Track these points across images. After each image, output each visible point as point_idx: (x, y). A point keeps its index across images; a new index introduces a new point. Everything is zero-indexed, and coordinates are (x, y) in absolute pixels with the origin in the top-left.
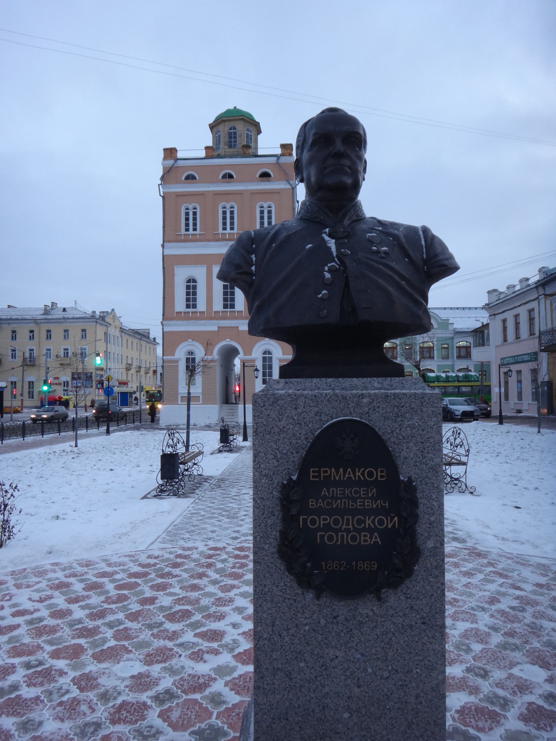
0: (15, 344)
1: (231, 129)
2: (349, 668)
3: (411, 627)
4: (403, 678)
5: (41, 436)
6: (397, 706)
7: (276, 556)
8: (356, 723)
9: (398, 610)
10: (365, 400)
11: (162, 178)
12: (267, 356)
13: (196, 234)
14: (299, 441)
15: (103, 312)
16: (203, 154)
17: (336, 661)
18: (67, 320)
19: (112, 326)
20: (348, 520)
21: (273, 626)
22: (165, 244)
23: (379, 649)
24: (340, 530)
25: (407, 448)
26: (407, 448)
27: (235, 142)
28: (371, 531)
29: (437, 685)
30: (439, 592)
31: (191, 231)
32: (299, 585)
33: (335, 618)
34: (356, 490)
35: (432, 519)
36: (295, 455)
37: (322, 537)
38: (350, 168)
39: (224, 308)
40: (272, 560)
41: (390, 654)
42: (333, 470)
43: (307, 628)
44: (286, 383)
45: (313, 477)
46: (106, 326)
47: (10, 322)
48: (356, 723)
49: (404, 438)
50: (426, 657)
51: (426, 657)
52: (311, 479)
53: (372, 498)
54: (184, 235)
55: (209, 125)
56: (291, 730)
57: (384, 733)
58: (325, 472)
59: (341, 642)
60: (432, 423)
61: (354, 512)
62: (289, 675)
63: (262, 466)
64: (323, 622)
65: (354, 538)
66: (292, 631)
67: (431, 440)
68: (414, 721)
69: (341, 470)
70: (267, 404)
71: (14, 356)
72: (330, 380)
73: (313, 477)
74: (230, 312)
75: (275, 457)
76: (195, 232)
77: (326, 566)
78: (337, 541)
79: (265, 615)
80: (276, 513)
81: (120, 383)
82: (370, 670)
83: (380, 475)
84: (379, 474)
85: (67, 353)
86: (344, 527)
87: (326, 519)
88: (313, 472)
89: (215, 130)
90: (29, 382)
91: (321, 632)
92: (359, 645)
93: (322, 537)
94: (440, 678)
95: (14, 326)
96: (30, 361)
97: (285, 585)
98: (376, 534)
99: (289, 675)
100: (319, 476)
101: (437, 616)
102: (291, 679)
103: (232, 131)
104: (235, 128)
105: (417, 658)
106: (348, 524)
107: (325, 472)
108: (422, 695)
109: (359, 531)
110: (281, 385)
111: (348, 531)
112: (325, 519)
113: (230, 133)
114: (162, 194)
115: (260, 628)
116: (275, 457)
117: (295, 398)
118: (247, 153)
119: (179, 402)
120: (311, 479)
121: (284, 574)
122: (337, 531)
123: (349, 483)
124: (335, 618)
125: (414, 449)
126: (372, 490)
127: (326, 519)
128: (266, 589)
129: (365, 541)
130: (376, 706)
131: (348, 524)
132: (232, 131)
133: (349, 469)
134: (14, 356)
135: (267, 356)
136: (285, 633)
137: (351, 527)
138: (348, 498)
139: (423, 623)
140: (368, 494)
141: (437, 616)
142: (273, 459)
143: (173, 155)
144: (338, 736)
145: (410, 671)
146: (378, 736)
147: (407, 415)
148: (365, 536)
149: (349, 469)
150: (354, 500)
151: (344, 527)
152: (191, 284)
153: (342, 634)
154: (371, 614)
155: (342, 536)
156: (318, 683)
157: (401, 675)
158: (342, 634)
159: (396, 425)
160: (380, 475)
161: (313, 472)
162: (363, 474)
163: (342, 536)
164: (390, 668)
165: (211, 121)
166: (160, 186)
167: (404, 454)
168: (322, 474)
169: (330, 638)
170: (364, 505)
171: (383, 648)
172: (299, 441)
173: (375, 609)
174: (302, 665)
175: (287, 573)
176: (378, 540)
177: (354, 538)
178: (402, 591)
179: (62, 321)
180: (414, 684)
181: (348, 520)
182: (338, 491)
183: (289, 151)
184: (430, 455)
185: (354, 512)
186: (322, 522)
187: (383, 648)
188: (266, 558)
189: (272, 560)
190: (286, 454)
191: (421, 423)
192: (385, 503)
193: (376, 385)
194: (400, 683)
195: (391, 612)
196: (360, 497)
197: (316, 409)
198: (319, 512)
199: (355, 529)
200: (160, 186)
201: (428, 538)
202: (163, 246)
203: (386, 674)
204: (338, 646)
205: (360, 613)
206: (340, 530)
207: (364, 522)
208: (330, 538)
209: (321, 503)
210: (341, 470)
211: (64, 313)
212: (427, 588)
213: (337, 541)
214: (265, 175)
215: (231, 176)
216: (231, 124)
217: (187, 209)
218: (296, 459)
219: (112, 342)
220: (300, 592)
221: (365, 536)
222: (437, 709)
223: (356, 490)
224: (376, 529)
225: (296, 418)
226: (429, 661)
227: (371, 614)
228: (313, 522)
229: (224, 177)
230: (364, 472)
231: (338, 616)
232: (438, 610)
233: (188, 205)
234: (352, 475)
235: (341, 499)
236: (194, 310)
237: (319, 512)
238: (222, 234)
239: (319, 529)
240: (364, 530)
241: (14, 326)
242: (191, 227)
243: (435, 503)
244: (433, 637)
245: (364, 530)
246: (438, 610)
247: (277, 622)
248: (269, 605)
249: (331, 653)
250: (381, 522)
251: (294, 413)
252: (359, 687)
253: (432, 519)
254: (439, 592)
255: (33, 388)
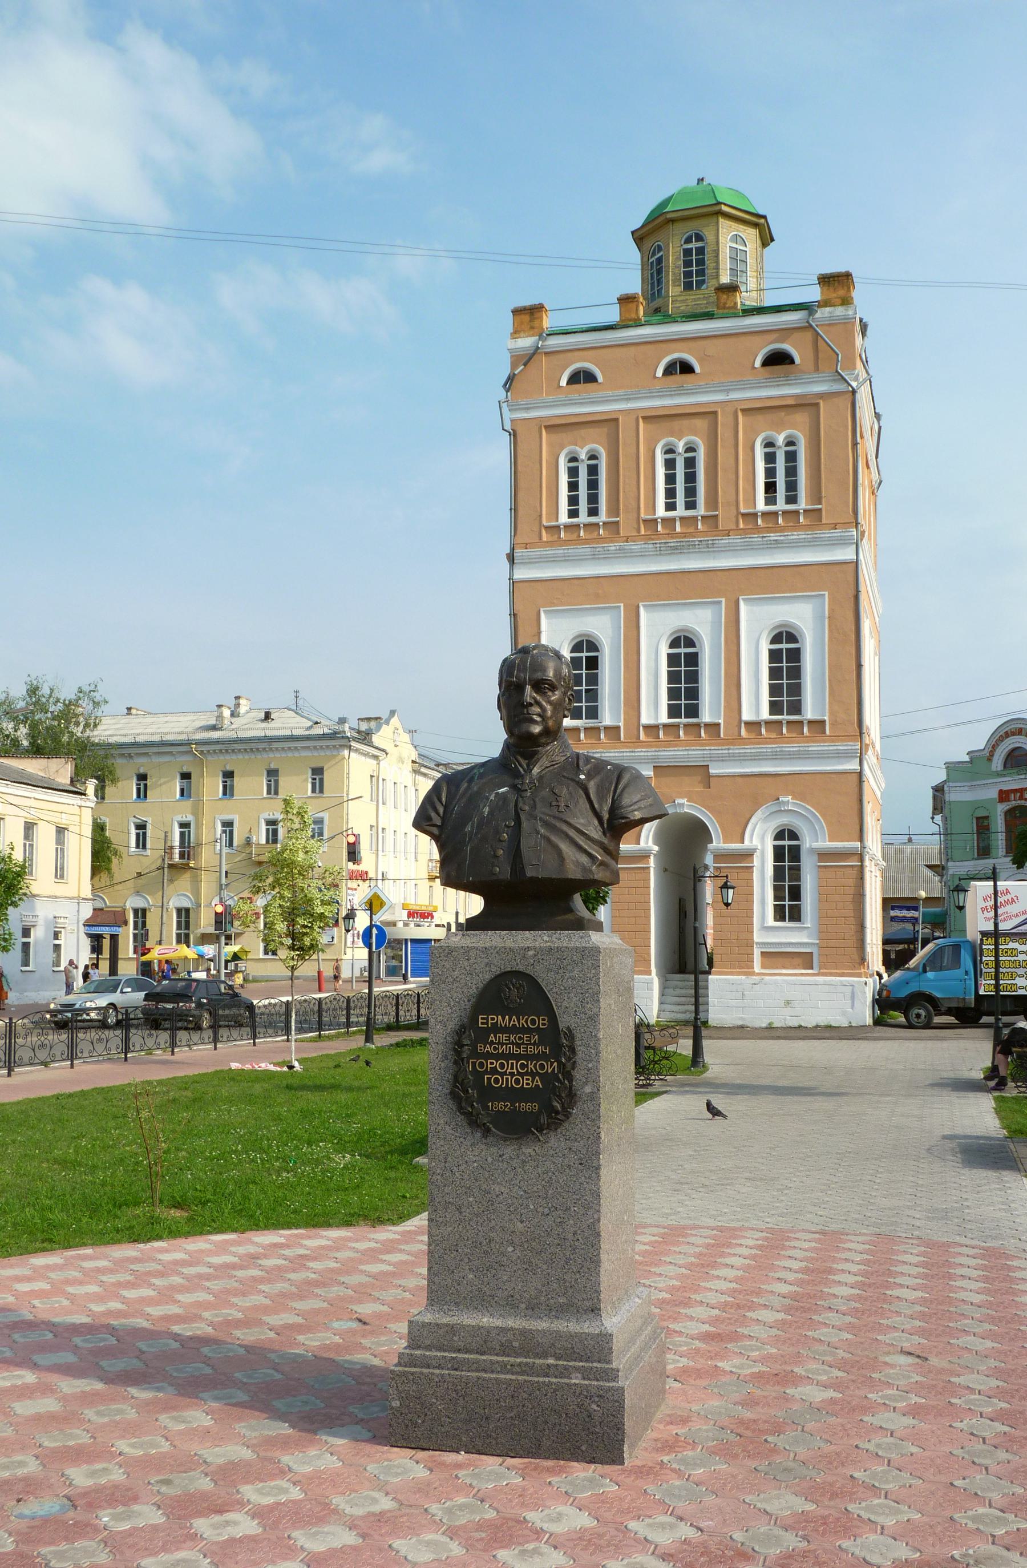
0: (146, 812)
1: (688, 240)
2: (513, 1204)
3: (569, 1167)
4: (562, 1216)
5: (211, 1046)
6: (556, 1242)
7: (449, 1097)
8: (519, 1257)
9: (558, 1150)
10: (531, 953)
11: (510, 383)
12: (786, 843)
13: (597, 525)
14: (471, 990)
15: (369, 719)
16: (613, 315)
17: (501, 1197)
18: (275, 745)
19: (392, 757)
20: (512, 1064)
21: (445, 1162)
22: (518, 553)
23: (540, 1187)
24: (505, 1073)
25: (569, 998)
26: (569, 998)
27: (701, 273)
28: (533, 1075)
29: (593, 1223)
30: (595, 1135)
31: (583, 518)
32: (469, 1124)
33: (500, 1156)
34: (520, 1037)
35: (590, 1065)
36: (467, 1003)
37: (489, 1079)
38: (539, 715)
39: (670, 715)
40: (445, 1101)
41: (550, 1192)
42: (500, 1017)
43: (476, 1164)
44: (463, 935)
45: (482, 1023)
46: (376, 757)
47: (133, 751)
48: (519, 1257)
49: (565, 989)
50: (583, 1196)
51: (583, 1196)
52: (480, 1025)
53: (534, 1044)
54: (566, 527)
55: (633, 233)
56: (461, 1261)
57: (545, 1267)
58: (493, 1019)
59: (506, 1179)
60: (592, 975)
61: (518, 1057)
62: (459, 1209)
63: (437, 1013)
64: (490, 1159)
65: (517, 1082)
66: (462, 1168)
67: (590, 991)
68: (572, 1257)
69: (507, 1017)
70: (442, 955)
71: (142, 842)
72: (504, 933)
73: (482, 1023)
74: (686, 725)
75: (449, 1005)
76: (593, 519)
77: (492, 1106)
78: (502, 1083)
79: (438, 1152)
80: (449, 1057)
81: (410, 915)
82: (532, 1207)
83: (542, 1022)
84: (541, 1022)
85: (275, 832)
86: (509, 1071)
87: (493, 1063)
88: (482, 1019)
89: (648, 244)
90: (179, 911)
91: (488, 1169)
92: (522, 1182)
93: (489, 1079)
94: (596, 1216)
95: (142, 764)
96: (182, 855)
97: (457, 1124)
98: (537, 1078)
99: (459, 1209)
100: (487, 1023)
101: (594, 1157)
102: (461, 1213)
103: (693, 245)
104: (699, 238)
105: (574, 1197)
106: (512, 1068)
107: (493, 1019)
108: (579, 1232)
109: (522, 1075)
110: (459, 937)
111: (512, 1074)
112: (492, 1063)
113: (687, 252)
114: (508, 427)
115: (434, 1164)
116: (449, 1005)
117: (467, 950)
118: (730, 304)
119: (757, 969)
120: (480, 1025)
121: (455, 1114)
122: (502, 1075)
123: (514, 1030)
124: (500, 1156)
125: (575, 999)
126: (534, 1036)
127: (493, 1063)
128: (440, 1128)
129: (528, 1084)
130: (537, 1240)
131: (512, 1068)
132: (693, 245)
133: (514, 1017)
134: (142, 842)
135: (786, 843)
136: (455, 1169)
137: (515, 1071)
138: (513, 1043)
139: (581, 1164)
140: (530, 1040)
141: (594, 1157)
142: (446, 1007)
143: (536, 323)
144: (502, 1268)
145: (568, 1209)
146: (539, 1270)
147: (569, 967)
148: (527, 1079)
149: (514, 1017)
150: (518, 1046)
151: (509, 1071)
152: (584, 654)
153: (507, 1172)
154: (533, 1153)
155: (507, 1079)
156: (485, 1217)
157: (560, 1212)
158: (507, 1172)
159: (558, 977)
160: (542, 1022)
161: (482, 1019)
162: (526, 1022)
163: (507, 1079)
164: (550, 1205)
165: (638, 224)
166: (504, 406)
167: (565, 1004)
168: (490, 1021)
169: (496, 1175)
170: (527, 1051)
171: (544, 1186)
172: (471, 990)
173: (536, 1149)
174: (471, 1199)
175: (458, 1114)
176: (539, 1083)
177: (517, 1082)
178: (561, 1133)
179: (261, 746)
180: (571, 1222)
181: (512, 1064)
182: (503, 1037)
183: (841, 292)
184: (589, 1006)
185: (518, 1057)
186: (489, 1066)
187: (544, 1186)
188: (440, 1098)
189: (445, 1101)
190: (459, 1002)
191: (581, 975)
192: (546, 1049)
193: (546, 938)
194: (559, 1220)
195: (552, 1152)
196: (523, 1043)
197: (487, 961)
198: (488, 1056)
199: (519, 1073)
200: (504, 406)
201: (586, 1083)
202: (511, 558)
203: (546, 1211)
204: (503, 1183)
205: (523, 1153)
206: (505, 1073)
207: (527, 1066)
208: (497, 1081)
209: (489, 1049)
210: (507, 1017)
211: (264, 725)
212: (585, 1130)
213: (502, 1083)
214: (778, 359)
215: (686, 368)
216: (689, 229)
217: (574, 459)
218: (467, 1007)
219: (390, 802)
220: (469, 1131)
221: (527, 1079)
222: (592, 1246)
223: (520, 1037)
224: (538, 1074)
225: (468, 968)
226: (586, 1200)
227: (533, 1153)
228: (481, 1065)
229: (669, 371)
230: (527, 1019)
231: (503, 1155)
232: (594, 1152)
233: (578, 448)
234: (516, 1023)
235: (507, 1044)
236: (591, 723)
237: (488, 1056)
238: (664, 520)
239: (486, 1072)
240: (527, 1073)
241: (142, 764)
242: (583, 506)
243: (593, 1051)
244: (590, 1178)
245: (527, 1073)
246: (594, 1152)
247: (449, 1159)
248: (442, 1143)
249: (497, 1189)
250: (542, 1067)
251: (466, 963)
252: (522, 1222)
253: (590, 1065)
254: (595, 1135)
255: (187, 927)
